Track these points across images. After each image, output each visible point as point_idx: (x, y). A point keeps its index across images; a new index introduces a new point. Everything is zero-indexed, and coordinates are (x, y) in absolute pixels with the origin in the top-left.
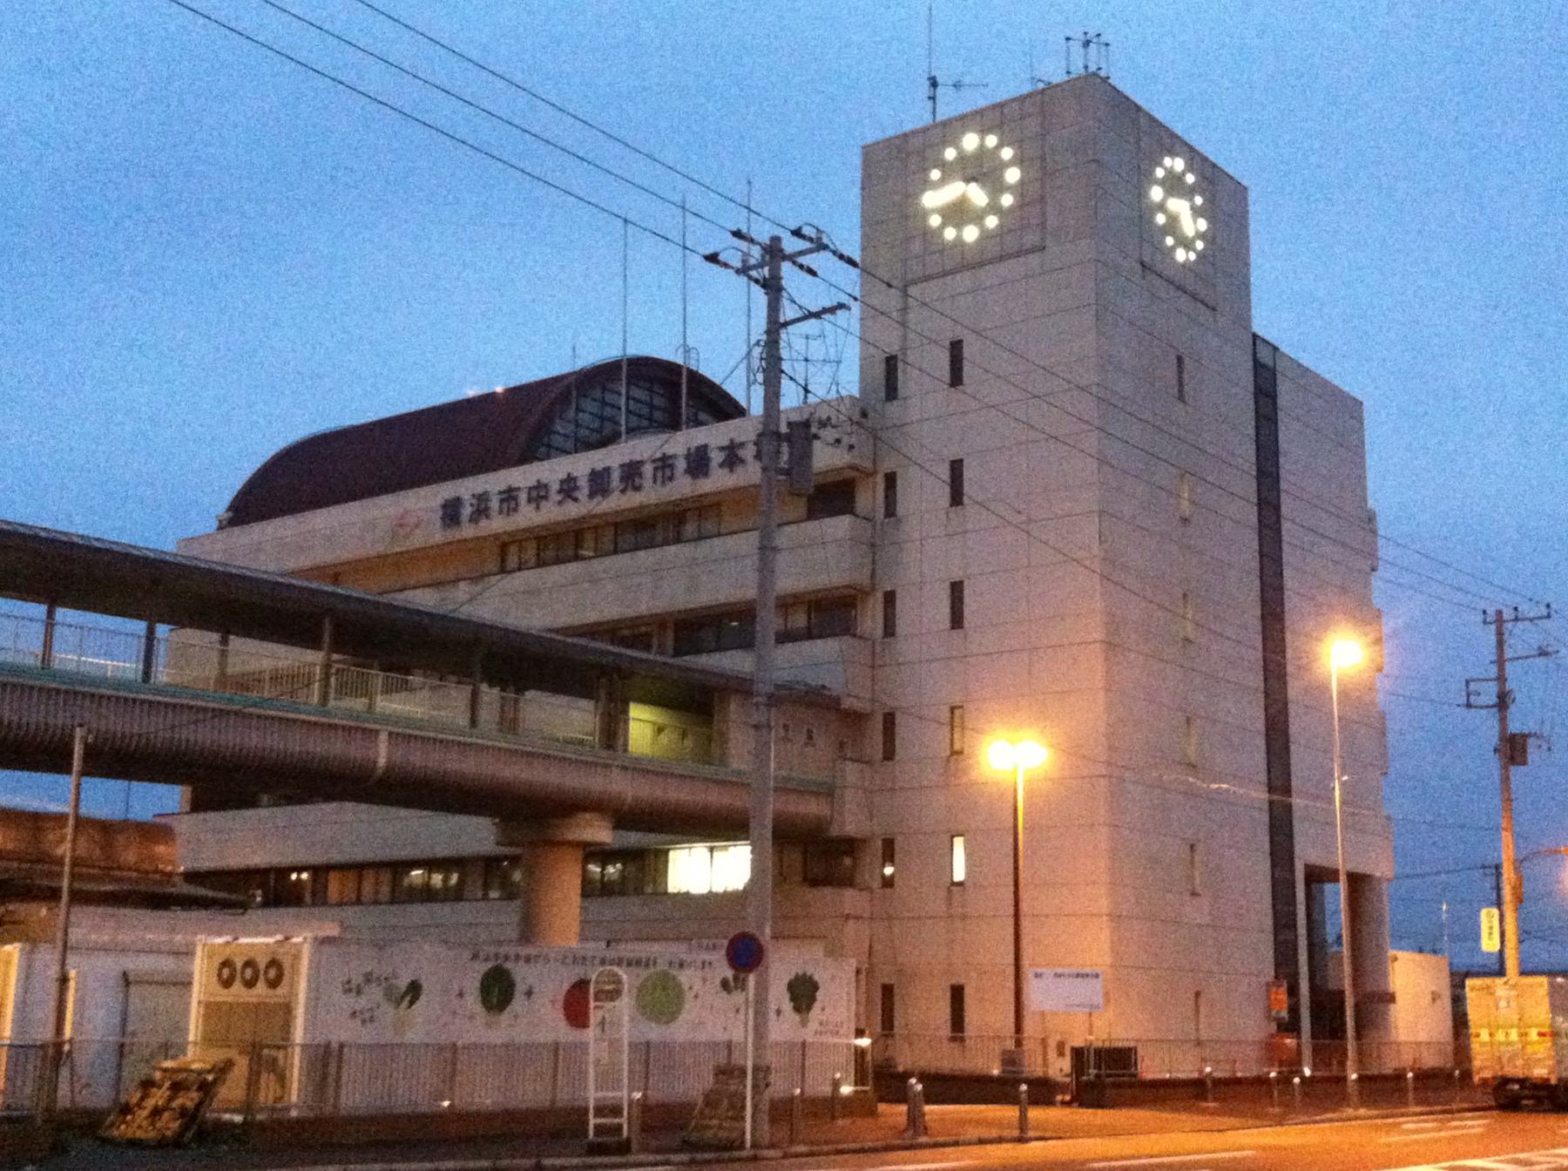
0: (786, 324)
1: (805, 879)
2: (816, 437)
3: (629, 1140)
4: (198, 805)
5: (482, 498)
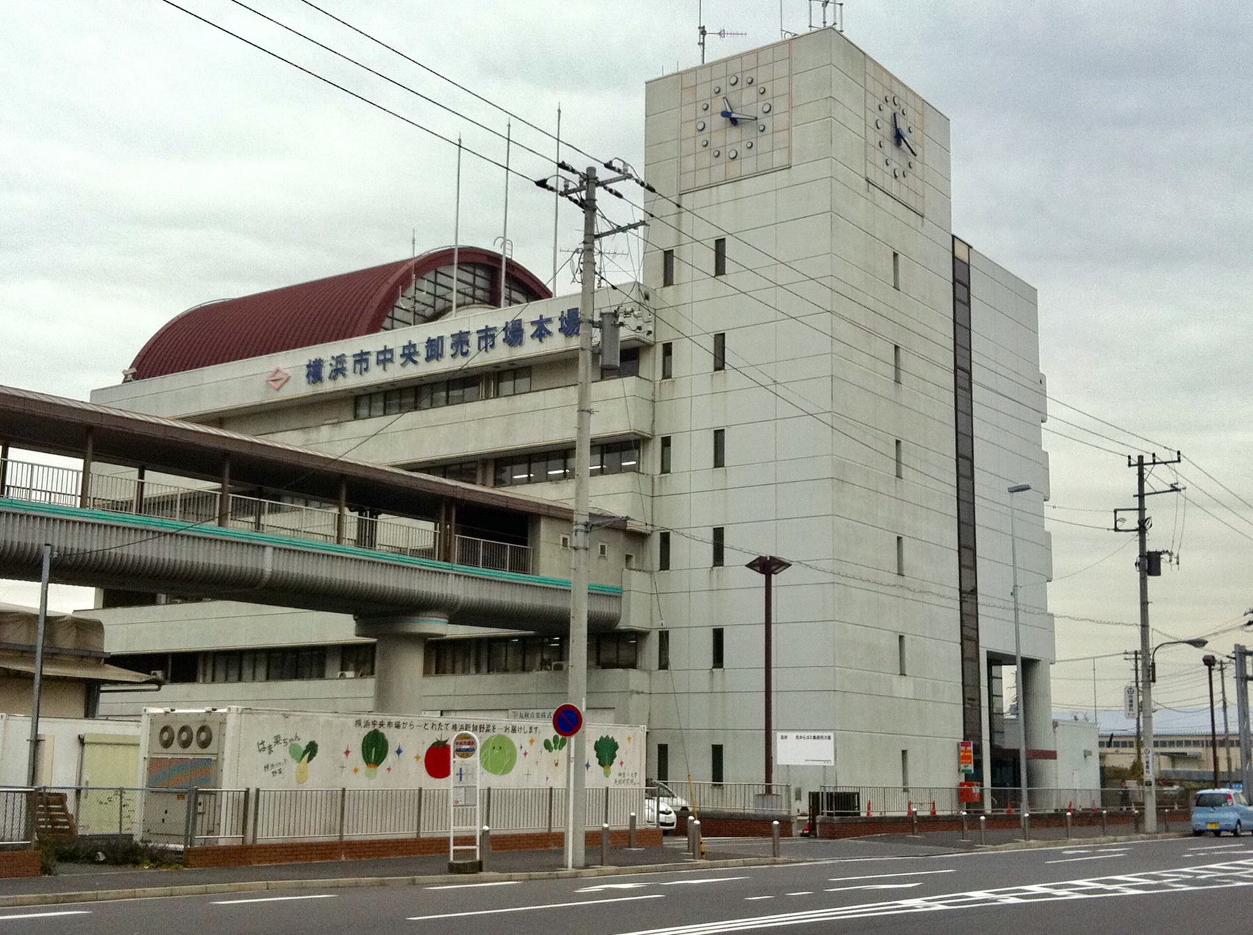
0: (599, 236)
1: (598, 664)
2: (622, 324)
3: (480, 862)
4: (112, 600)
5: (340, 359)
